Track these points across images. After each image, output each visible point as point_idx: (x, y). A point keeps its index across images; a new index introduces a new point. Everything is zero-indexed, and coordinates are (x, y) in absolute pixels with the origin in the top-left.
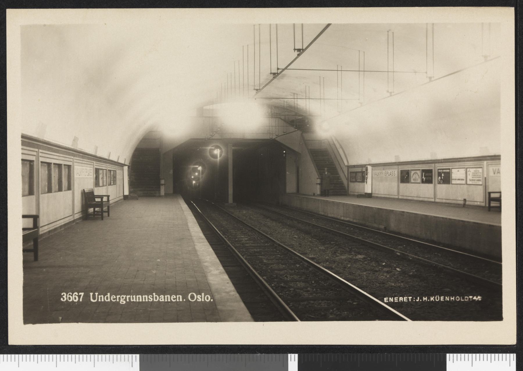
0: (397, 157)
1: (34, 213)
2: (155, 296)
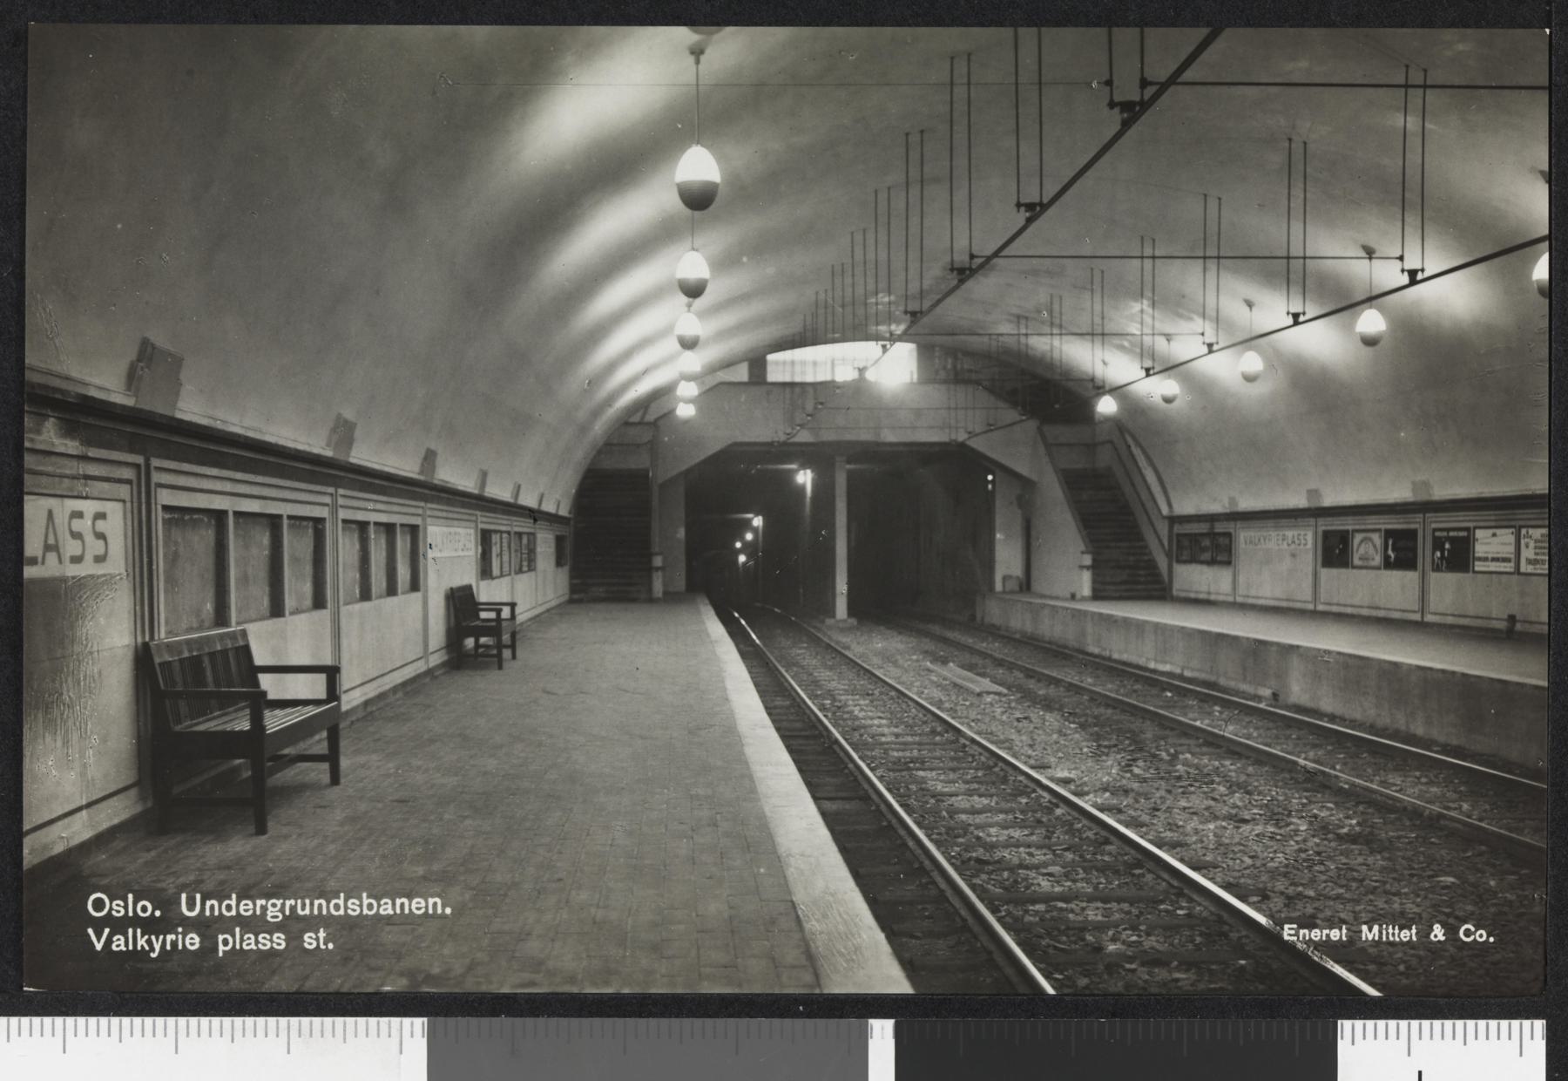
0: (1313, 493)
1: (328, 661)
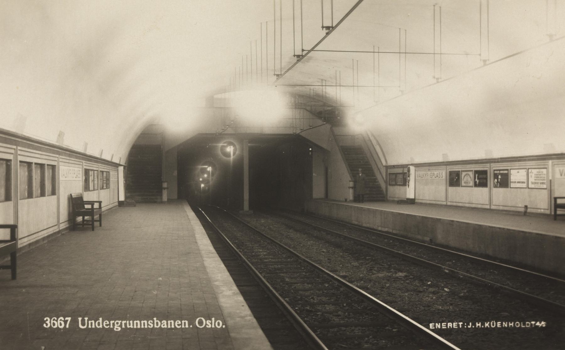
0: (445, 155)
1: (11, 222)
2: (155, 321)
